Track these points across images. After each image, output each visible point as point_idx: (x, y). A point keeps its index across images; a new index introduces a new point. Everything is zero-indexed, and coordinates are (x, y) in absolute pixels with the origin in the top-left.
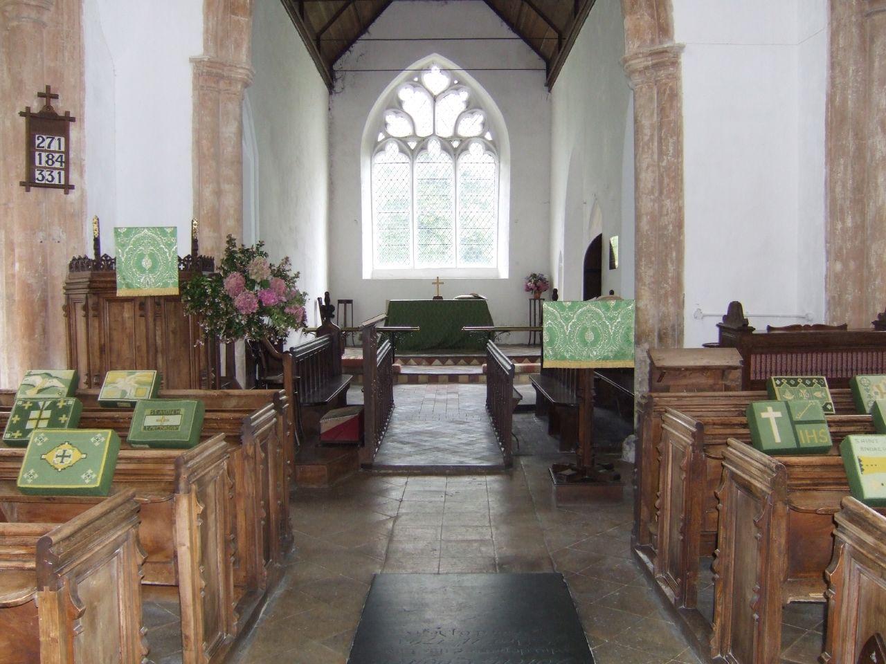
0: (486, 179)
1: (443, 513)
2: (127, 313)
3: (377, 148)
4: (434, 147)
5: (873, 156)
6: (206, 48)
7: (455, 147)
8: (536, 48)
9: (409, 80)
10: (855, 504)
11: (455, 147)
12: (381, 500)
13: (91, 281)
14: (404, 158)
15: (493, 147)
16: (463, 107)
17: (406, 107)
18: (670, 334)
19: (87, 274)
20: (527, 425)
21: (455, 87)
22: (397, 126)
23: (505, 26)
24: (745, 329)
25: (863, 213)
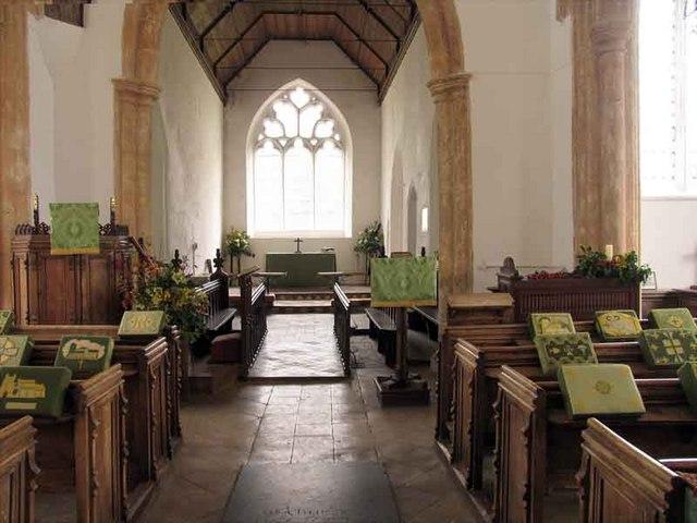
0: (335, 167)
1: (302, 406)
2: (59, 266)
3: (257, 145)
4: (299, 143)
5: (606, 152)
6: (124, 71)
7: (313, 145)
8: (370, 75)
9: (281, 97)
10: (596, 423)
11: (313, 145)
12: (252, 404)
13: (31, 243)
14: (277, 152)
15: (341, 145)
16: (319, 117)
17: (278, 117)
18: (464, 281)
19: (28, 237)
20: (363, 346)
21: (314, 102)
22: (272, 129)
23: (348, 60)
24: (516, 278)
25: (599, 192)
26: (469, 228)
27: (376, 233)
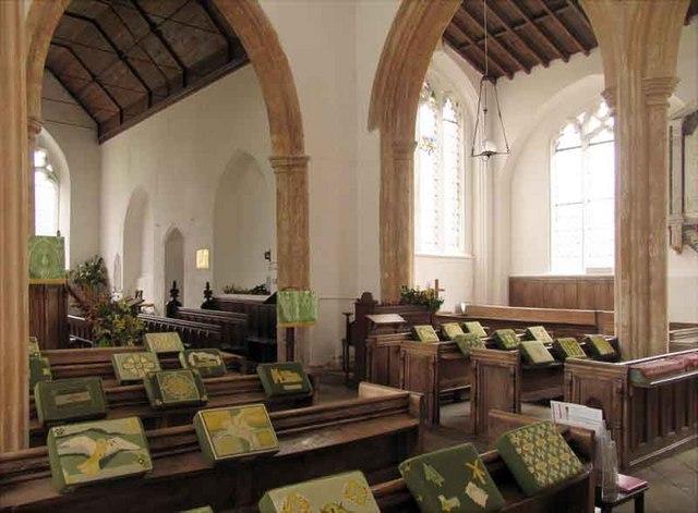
26: (306, 269)
27: (97, 267)
